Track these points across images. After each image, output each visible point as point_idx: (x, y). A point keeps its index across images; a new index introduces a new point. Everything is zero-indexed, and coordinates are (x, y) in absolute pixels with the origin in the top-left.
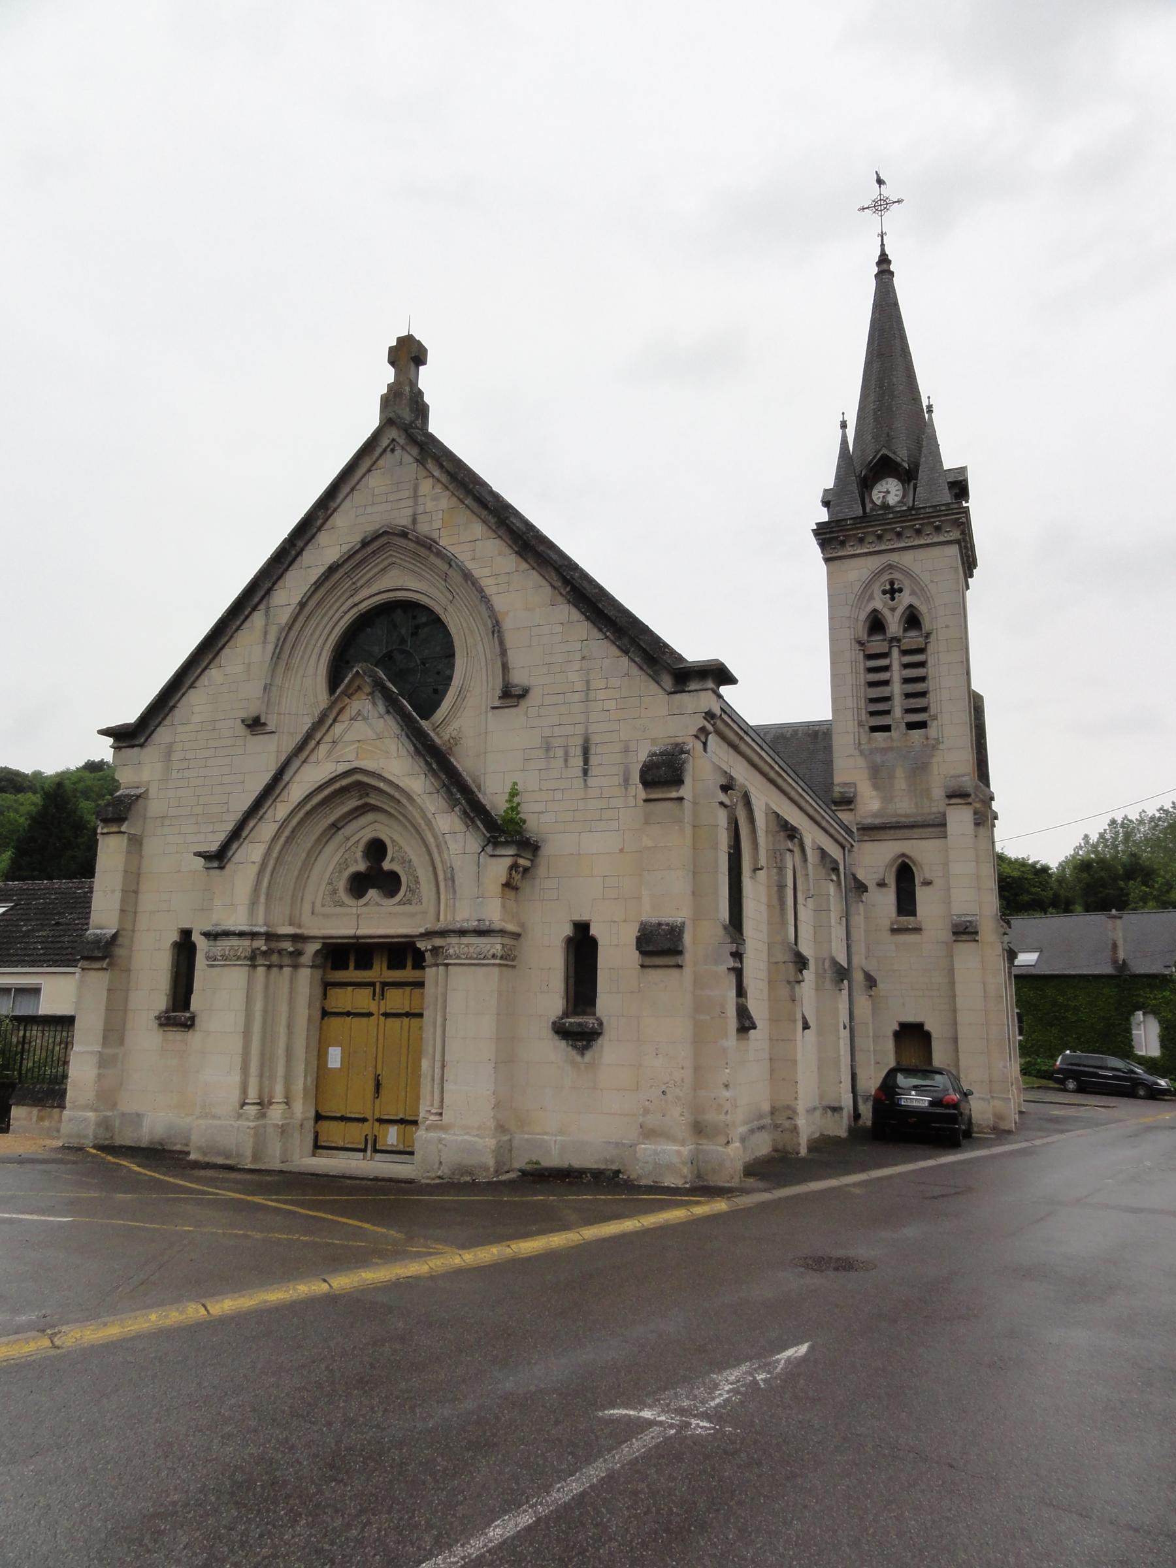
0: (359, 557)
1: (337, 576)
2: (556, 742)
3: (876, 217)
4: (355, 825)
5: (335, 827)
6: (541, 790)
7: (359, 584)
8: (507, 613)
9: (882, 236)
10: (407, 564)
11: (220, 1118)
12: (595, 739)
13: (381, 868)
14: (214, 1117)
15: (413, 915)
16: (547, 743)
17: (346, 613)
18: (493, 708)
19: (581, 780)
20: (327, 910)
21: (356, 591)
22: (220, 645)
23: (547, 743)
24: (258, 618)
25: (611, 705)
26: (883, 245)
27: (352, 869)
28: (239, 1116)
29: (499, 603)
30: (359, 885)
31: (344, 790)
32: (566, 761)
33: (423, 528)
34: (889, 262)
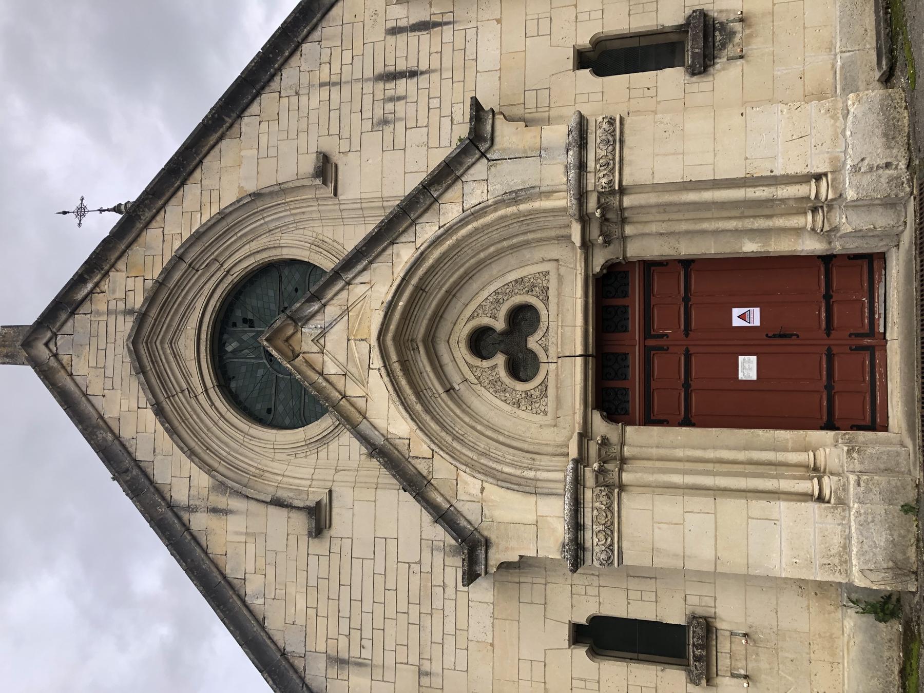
0: (154, 381)
1: (167, 407)
2: (379, 113)
3: (88, 215)
4: (450, 369)
5: (449, 390)
6: (427, 126)
7: (185, 386)
8: (241, 188)
9: (101, 211)
10: (175, 324)
11: (849, 538)
12: (379, 69)
13: (504, 333)
14: (846, 548)
15: (560, 278)
16: (379, 124)
17: (213, 404)
18: (335, 194)
19: (421, 78)
20: (550, 409)
21: (190, 389)
22: (220, 578)
23: (379, 124)
24: (199, 522)
25: (347, 55)
26: (108, 210)
27: (502, 373)
28: (842, 502)
29: (229, 198)
30: (522, 366)
31: (404, 363)
32: (399, 99)
33: (138, 301)
34: (120, 205)
